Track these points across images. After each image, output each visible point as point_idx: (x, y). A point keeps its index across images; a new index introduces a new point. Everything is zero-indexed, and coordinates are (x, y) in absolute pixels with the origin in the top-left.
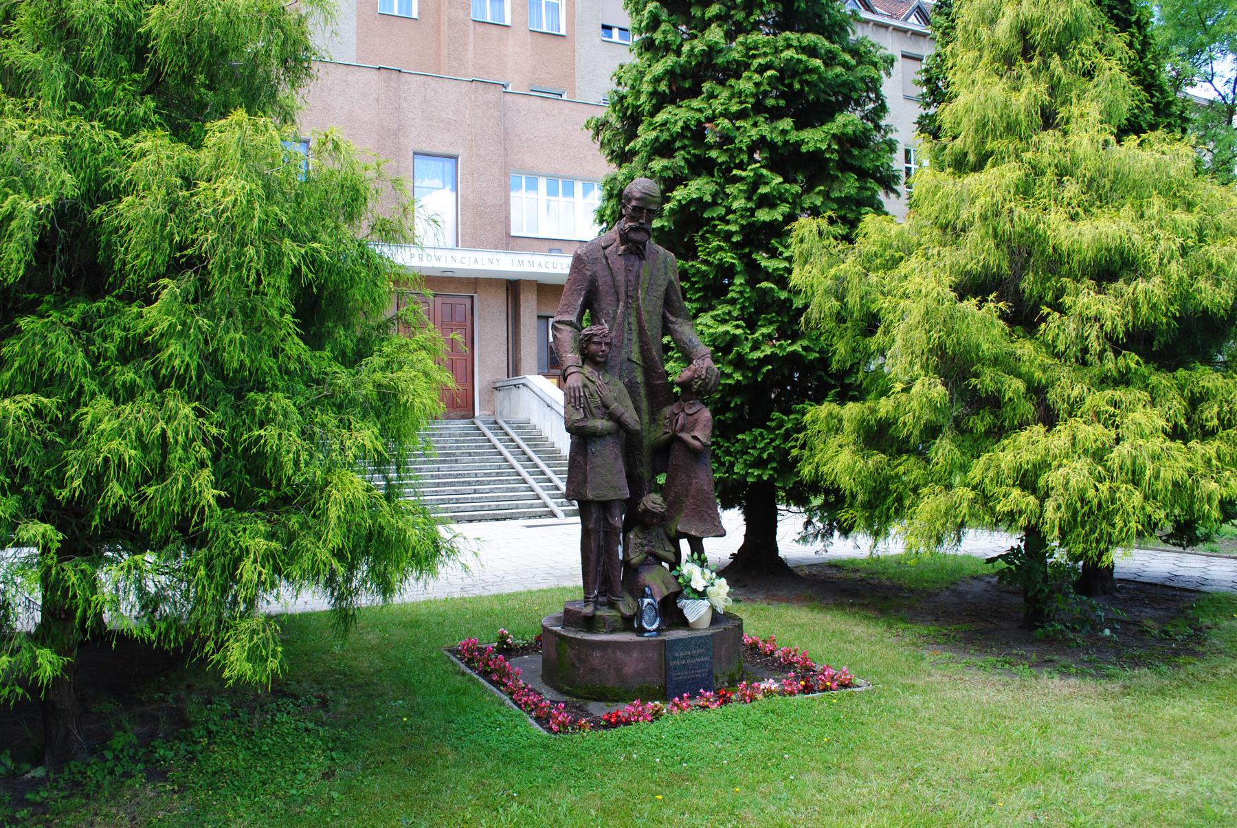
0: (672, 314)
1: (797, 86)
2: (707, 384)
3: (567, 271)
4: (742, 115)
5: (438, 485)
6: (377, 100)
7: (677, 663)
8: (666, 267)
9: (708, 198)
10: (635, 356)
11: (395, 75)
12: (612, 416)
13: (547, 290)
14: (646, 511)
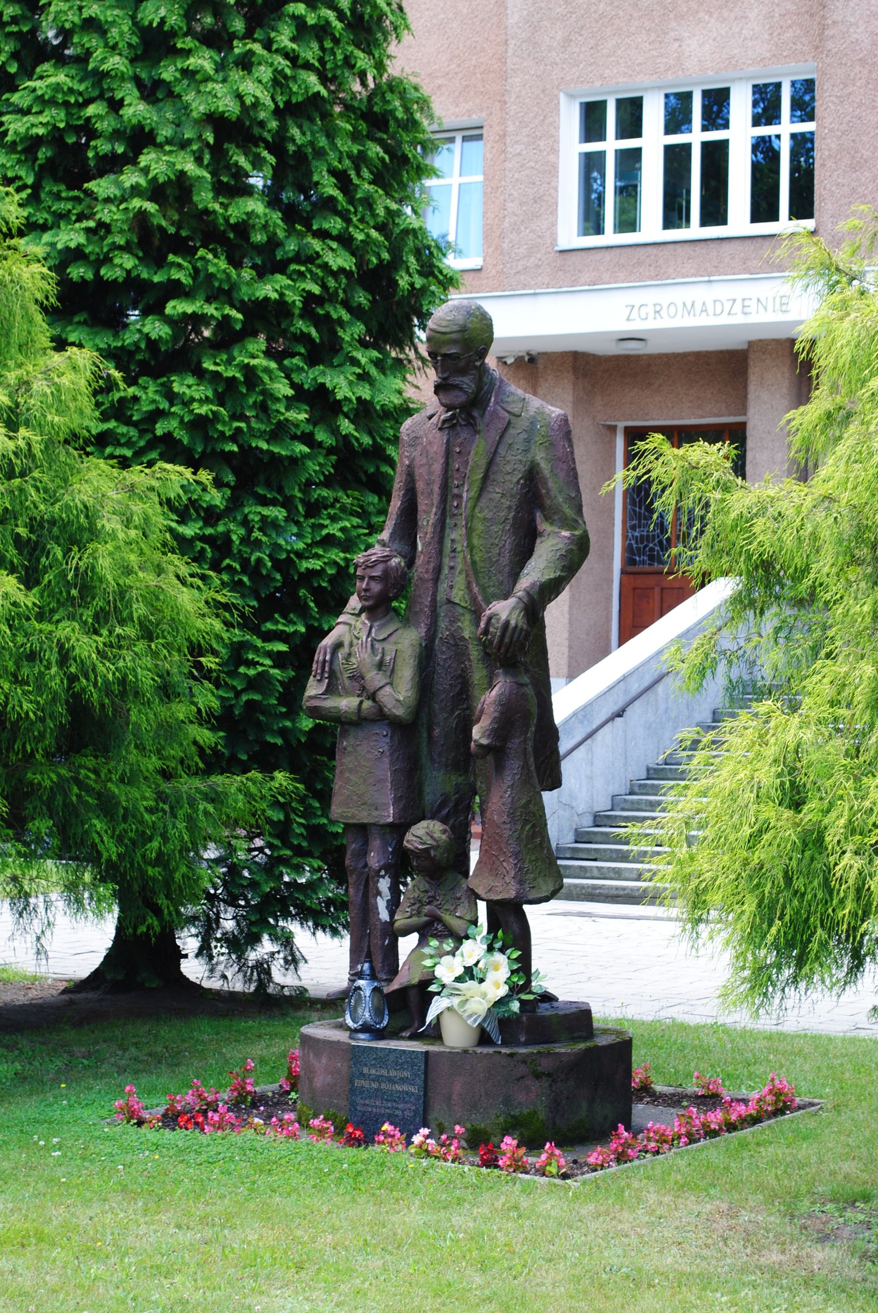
0: (547, 518)
7: (366, 1084)
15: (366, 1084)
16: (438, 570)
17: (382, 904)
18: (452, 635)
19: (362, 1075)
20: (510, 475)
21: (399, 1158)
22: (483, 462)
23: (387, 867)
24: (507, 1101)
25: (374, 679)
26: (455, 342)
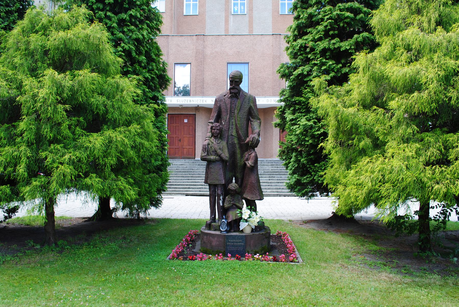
0: (252, 118)
1: (341, 25)
2: (253, 143)
3: (214, 103)
4: (320, 39)
5: (278, 183)
6: (272, 46)
7: (230, 244)
8: (249, 101)
9: (305, 73)
10: (234, 133)
11: (278, 36)
12: (217, 154)
13: (207, 110)
14: (229, 189)
15: (230, 244)
16: (229, 128)
17: (221, 202)
18: (232, 143)
19: (229, 242)
20: (246, 109)
21: (248, 262)
22: (240, 105)
23: (222, 194)
24: (262, 245)
25: (219, 151)
26: (238, 78)
